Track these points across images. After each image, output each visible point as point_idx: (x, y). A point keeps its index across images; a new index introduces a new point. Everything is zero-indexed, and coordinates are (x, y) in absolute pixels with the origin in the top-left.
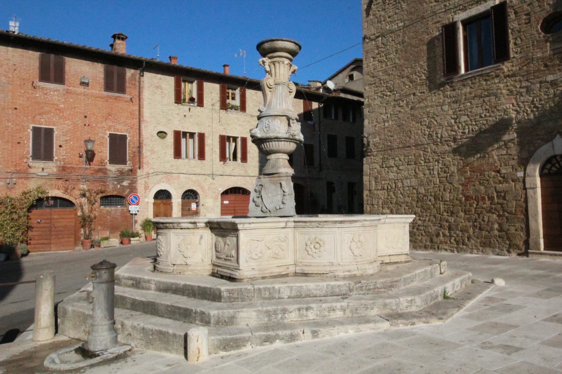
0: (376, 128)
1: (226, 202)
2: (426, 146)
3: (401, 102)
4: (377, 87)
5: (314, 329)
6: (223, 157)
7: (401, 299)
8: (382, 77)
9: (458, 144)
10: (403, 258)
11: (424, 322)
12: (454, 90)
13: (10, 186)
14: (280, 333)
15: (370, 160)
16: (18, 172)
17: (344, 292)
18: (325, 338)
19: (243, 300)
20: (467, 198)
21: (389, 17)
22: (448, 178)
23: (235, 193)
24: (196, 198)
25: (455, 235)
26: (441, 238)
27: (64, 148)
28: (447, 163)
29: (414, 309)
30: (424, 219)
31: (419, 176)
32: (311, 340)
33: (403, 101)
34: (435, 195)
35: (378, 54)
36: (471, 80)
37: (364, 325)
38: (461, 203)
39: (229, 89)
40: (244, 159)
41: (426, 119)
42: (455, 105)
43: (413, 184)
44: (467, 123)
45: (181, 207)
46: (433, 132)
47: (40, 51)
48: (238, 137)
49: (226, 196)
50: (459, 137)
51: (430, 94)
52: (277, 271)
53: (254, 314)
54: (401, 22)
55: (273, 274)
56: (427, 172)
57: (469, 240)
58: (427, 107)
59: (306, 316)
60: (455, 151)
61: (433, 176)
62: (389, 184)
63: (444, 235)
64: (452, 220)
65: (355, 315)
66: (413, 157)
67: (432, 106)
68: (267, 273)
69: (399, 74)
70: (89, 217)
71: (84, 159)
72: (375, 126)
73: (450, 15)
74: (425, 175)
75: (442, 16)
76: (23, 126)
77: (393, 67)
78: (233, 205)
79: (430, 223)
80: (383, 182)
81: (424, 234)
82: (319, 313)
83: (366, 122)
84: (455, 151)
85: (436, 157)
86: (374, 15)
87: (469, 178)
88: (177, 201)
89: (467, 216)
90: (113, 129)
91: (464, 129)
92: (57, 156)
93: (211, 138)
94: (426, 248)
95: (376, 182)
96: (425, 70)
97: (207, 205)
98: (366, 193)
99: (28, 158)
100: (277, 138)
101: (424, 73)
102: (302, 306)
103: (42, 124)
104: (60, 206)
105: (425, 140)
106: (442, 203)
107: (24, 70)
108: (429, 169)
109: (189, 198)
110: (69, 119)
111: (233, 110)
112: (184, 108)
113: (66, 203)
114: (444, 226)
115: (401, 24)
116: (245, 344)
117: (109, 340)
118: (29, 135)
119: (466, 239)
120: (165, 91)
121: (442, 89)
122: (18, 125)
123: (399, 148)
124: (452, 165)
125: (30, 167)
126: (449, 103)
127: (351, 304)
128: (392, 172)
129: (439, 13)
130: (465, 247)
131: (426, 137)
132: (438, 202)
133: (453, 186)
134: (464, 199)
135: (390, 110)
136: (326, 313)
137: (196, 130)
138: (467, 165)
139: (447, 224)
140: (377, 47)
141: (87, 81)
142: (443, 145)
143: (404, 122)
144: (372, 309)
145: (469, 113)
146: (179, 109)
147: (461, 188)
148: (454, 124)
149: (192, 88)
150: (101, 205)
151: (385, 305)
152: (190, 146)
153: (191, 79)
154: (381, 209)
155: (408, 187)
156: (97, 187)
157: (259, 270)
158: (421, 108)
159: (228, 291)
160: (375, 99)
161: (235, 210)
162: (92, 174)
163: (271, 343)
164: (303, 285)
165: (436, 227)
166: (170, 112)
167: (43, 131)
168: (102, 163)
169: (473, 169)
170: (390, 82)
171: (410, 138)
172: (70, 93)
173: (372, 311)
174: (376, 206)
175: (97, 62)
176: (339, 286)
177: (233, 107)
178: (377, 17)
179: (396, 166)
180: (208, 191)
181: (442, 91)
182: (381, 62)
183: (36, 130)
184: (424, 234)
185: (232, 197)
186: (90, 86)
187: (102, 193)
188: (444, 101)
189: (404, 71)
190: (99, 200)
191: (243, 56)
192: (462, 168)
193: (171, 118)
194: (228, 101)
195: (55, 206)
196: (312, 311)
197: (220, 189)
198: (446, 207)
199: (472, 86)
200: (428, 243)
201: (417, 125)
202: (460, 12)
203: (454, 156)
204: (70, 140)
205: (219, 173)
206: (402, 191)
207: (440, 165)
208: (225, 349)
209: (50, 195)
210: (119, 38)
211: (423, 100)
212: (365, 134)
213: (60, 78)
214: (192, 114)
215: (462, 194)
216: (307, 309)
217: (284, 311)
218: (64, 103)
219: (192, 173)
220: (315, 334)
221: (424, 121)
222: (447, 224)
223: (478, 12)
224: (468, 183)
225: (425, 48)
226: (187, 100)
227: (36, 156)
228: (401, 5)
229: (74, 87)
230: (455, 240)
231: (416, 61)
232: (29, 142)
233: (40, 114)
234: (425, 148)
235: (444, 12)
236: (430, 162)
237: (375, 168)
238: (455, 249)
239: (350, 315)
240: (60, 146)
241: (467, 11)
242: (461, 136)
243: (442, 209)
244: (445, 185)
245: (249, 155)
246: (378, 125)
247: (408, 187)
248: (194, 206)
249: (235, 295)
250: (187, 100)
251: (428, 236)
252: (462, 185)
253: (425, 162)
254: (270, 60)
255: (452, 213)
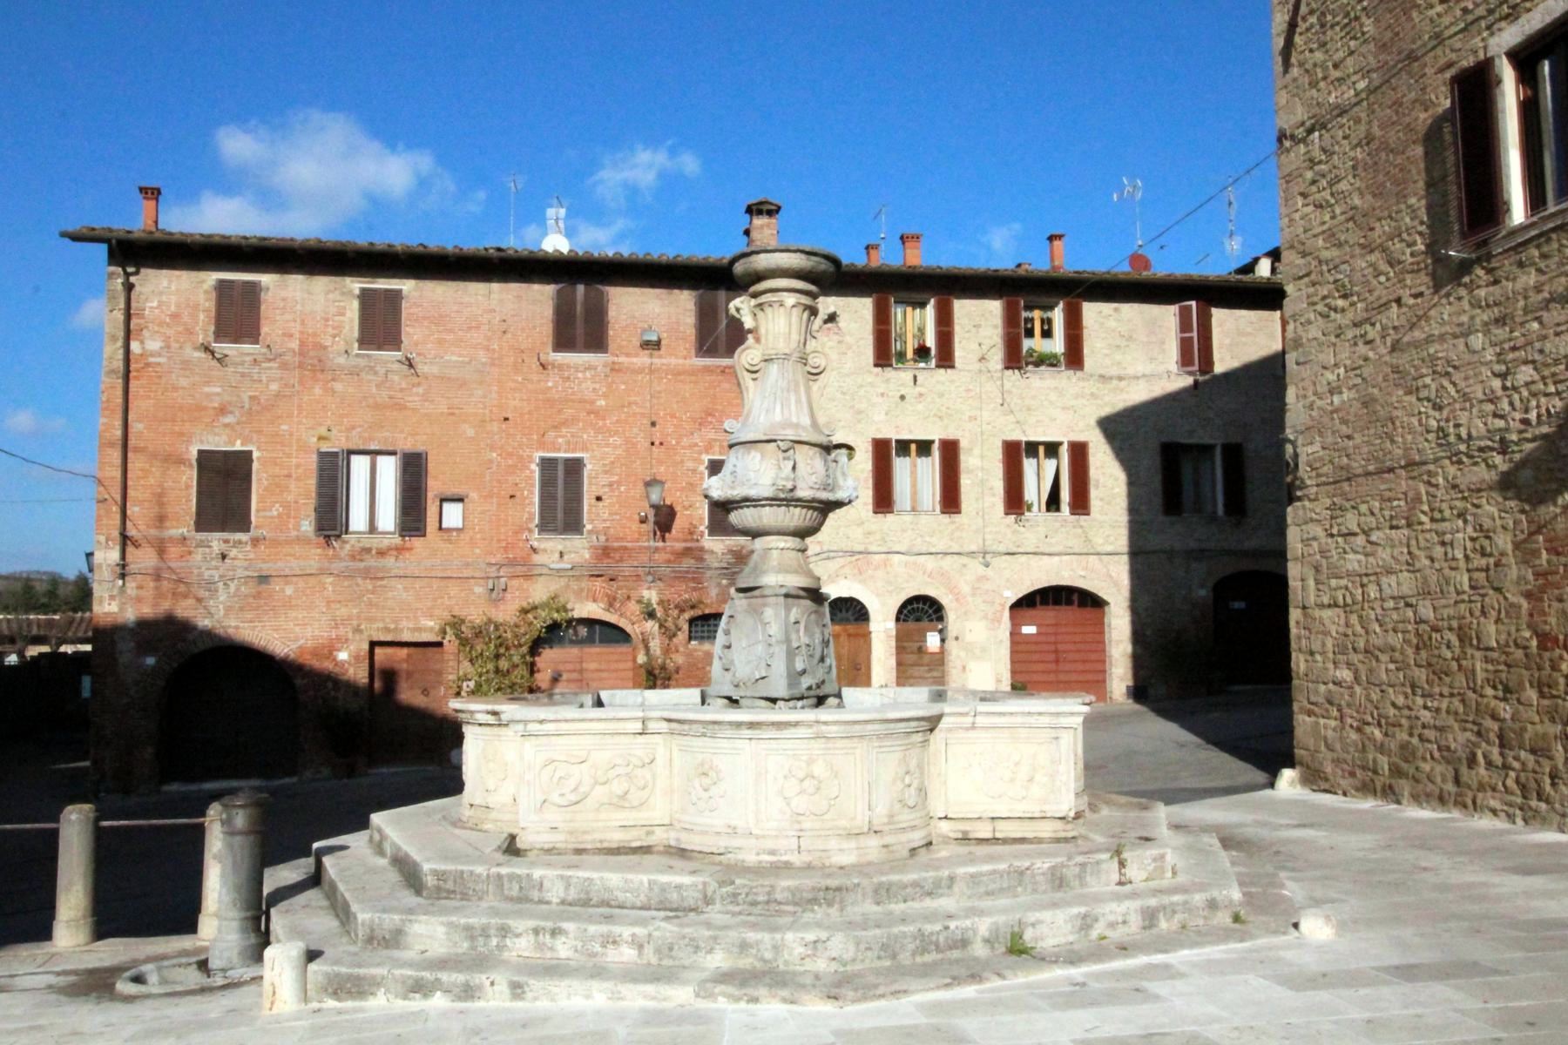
0: (1314, 413)
1: (1030, 630)
2: (1432, 467)
3: (1368, 327)
4: (1314, 284)
5: (516, 979)
6: (1015, 501)
7: (790, 936)
8: (1326, 254)
9: (1511, 460)
10: (1046, 830)
11: (784, 1000)
12: (1496, 282)
13: (494, 595)
14: (445, 977)
15: (1301, 512)
16: (512, 563)
17: (692, 903)
18: (538, 1003)
19: (465, 897)
20: (1546, 640)
21: (1336, 66)
22: (1492, 572)
23: (1057, 602)
24: (941, 619)
25: (1516, 765)
26: (1482, 771)
27: (606, 502)
28: (1487, 523)
29: (821, 965)
30: (1436, 704)
31: (1418, 565)
32: (508, 1004)
33: (1373, 325)
34: (1460, 628)
35: (1314, 182)
36: (1538, 247)
37: (631, 986)
38: (1526, 655)
39: (1029, 308)
40: (1081, 504)
41: (1428, 380)
42: (1499, 331)
43: (1405, 590)
44: (1534, 388)
45: (893, 643)
46: (1447, 420)
47: (556, 282)
48: (1060, 444)
49: (1031, 612)
50: (1514, 437)
51: (1436, 299)
52: (616, 838)
53: (441, 930)
54: (1363, 77)
55: (605, 845)
56: (1438, 551)
57: (1553, 784)
58: (1429, 340)
59: (551, 949)
60: (1507, 484)
61: (1454, 564)
62: (1347, 588)
63: (1489, 764)
64: (1505, 710)
65: (665, 962)
66: (1402, 503)
67: (1442, 338)
68: (588, 841)
69: (1362, 241)
70: (663, 668)
71: (650, 526)
72: (1311, 407)
73: (1478, 39)
74: (1432, 560)
75: (1458, 45)
76: (521, 457)
77: (1348, 220)
78: (1052, 639)
79: (1451, 721)
80: (1334, 582)
81: (1437, 754)
82: (580, 945)
83: (1291, 395)
84: (1507, 484)
85: (1458, 504)
86: (1301, 65)
87: (1544, 574)
88: (882, 626)
89: (1546, 702)
90: (717, 449)
91: (1527, 411)
92: (592, 521)
93: (976, 451)
94: (1442, 800)
95: (1317, 582)
96: (1422, 223)
97: (969, 638)
98: (1295, 615)
99: (530, 531)
100: (746, 499)
101: (1420, 234)
102: (542, 924)
103: (559, 450)
104: (601, 641)
105: (1429, 449)
106: (1478, 654)
107: (523, 330)
108: (1443, 544)
109: (918, 620)
110: (616, 433)
111: (1043, 368)
112: (899, 377)
113: (611, 634)
114: (1488, 730)
115: (1362, 85)
116: (374, 989)
117: (235, 952)
118: (531, 478)
119: (1548, 781)
120: (848, 339)
121: (1466, 279)
122: (510, 455)
123: (1368, 474)
124: (1499, 529)
125: (534, 550)
126: (1486, 324)
127: (656, 934)
128: (1356, 552)
129: (1450, 37)
130: (1543, 806)
131: (1431, 436)
132: (1469, 651)
133: (1506, 598)
134: (1534, 643)
135: (1344, 355)
136: (598, 948)
137: (935, 434)
138: (1538, 531)
139: (1495, 726)
140: (1311, 160)
141: (655, 338)
142: (1476, 464)
143: (1376, 391)
144: (710, 951)
145: (1537, 357)
146: (888, 381)
147: (1525, 604)
148: (1500, 393)
149: (923, 319)
150: (690, 638)
151: (744, 946)
152: (917, 479)
153: (918, 297)
154: (1331, 666)
155: (1393, 598)
156: (684, 593)
157: (571, 833)
158: (1416, 345)
159: (435, 873)
160: (1309, 322)
161: (1056, 651)
162: (669, 561)
163: (425, 996)
164: (595, 875)
165: (1468, 734)
166: (862, 392)
167: (561, 468)
168: (691, 533)
169: (1555, 544)
170: (1343, 267)
171: (1393, 441)
172: (619, 371)
173: (709, 957)
174: (1318, 657)
175: (680, 288)
176: (679, 887)
177: (1043, 361)
178: (1307, 71)
179: (1364, 532)
180: (970, 599)
181: (1465, 285)
182: (1321, 206)
183: (548, 465)
184: (1437, 754)
185: (1049, 614)
186: (663, 348)
187: (693, 607)
188: (1472, 318)
189: (1372, 229)
190: (686, 627)
191: (1132, 195)
192: (1525, 541)
193: (863, 406)
194: (1027, 344)
195: (589, 640)
196: (564, 939)
197: (1007, 594)
198: (1490, 667)
199: (1542, 265)
200: (1450, 787)
201: (1407, 398)
202: (1503, 24)
203: (1505, 499)
204: (619, 483)
205: (1002, 548)
206: (1379, 611)
207: (1470, 529)
208: (335, 994)
209: (576, 614)
210: (760, 212)
211: (1419, 318)
212: (1290, 434)
213: (596, 340)
214: (922, 390)
215: (1529, 626)
216: (555, 933)
217: (504, 931)
218: (605, 396)
219: (924, 550)
220: (517, 989)
221: (1425, 386)
222: (1495, 726)
223: (1548, 20)
224: (1542, 590)
225: (1419, 150)
226: (910, 354)
227: (548, 524)
228: (1361, 26)
229: (628, 355)
230: (1517, 781)
231: (1402, 197)
232: (532, 493)
233: (555, 427)
234: (1429, 473)
235: (1461, 31)
236: (1443, 520)
237: (1315, 539)
238: (1518, 812)
239: (654, 961)
240: (599, 499)
241: (1520, 21)
242: (1521, 432)
243: (1480, 676)
244: (1483, 596)
245: (1094, 494)
246: (1319, 403)
247: (1393, 598)
248: (933, 641)
249: (450, 885)
250: (910, 354)
251: (1448, 762)
252: (1528, 595)
253: (1433, 520)
254: (753, 302)
255: (1507, 690)
